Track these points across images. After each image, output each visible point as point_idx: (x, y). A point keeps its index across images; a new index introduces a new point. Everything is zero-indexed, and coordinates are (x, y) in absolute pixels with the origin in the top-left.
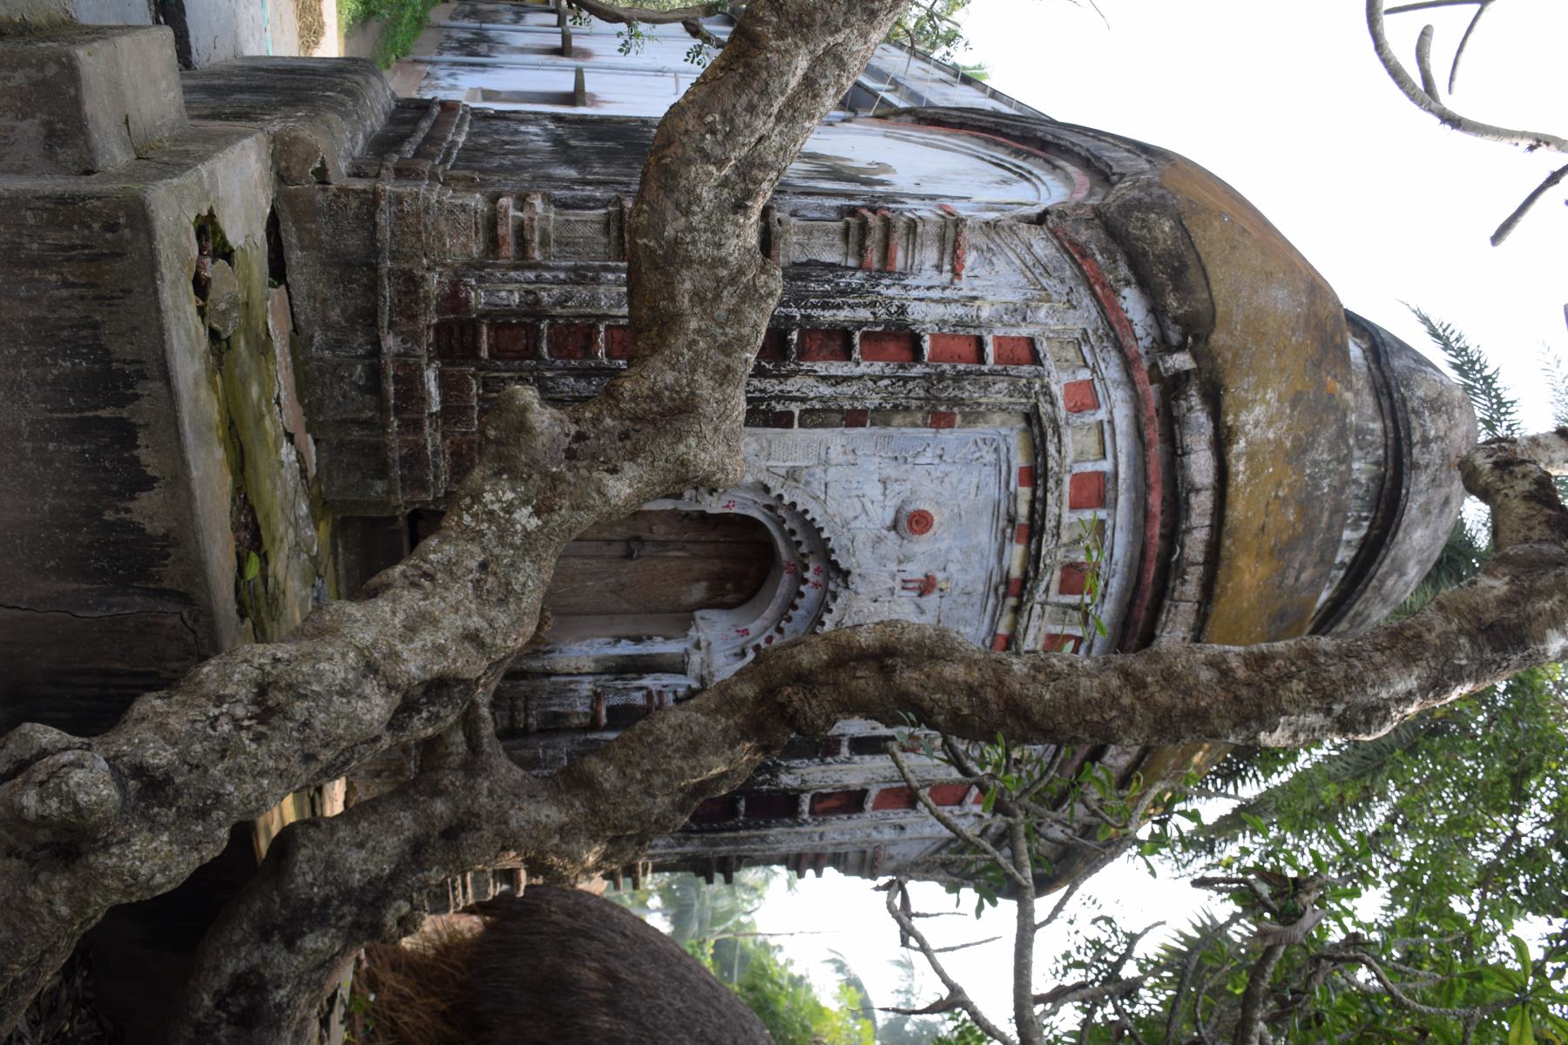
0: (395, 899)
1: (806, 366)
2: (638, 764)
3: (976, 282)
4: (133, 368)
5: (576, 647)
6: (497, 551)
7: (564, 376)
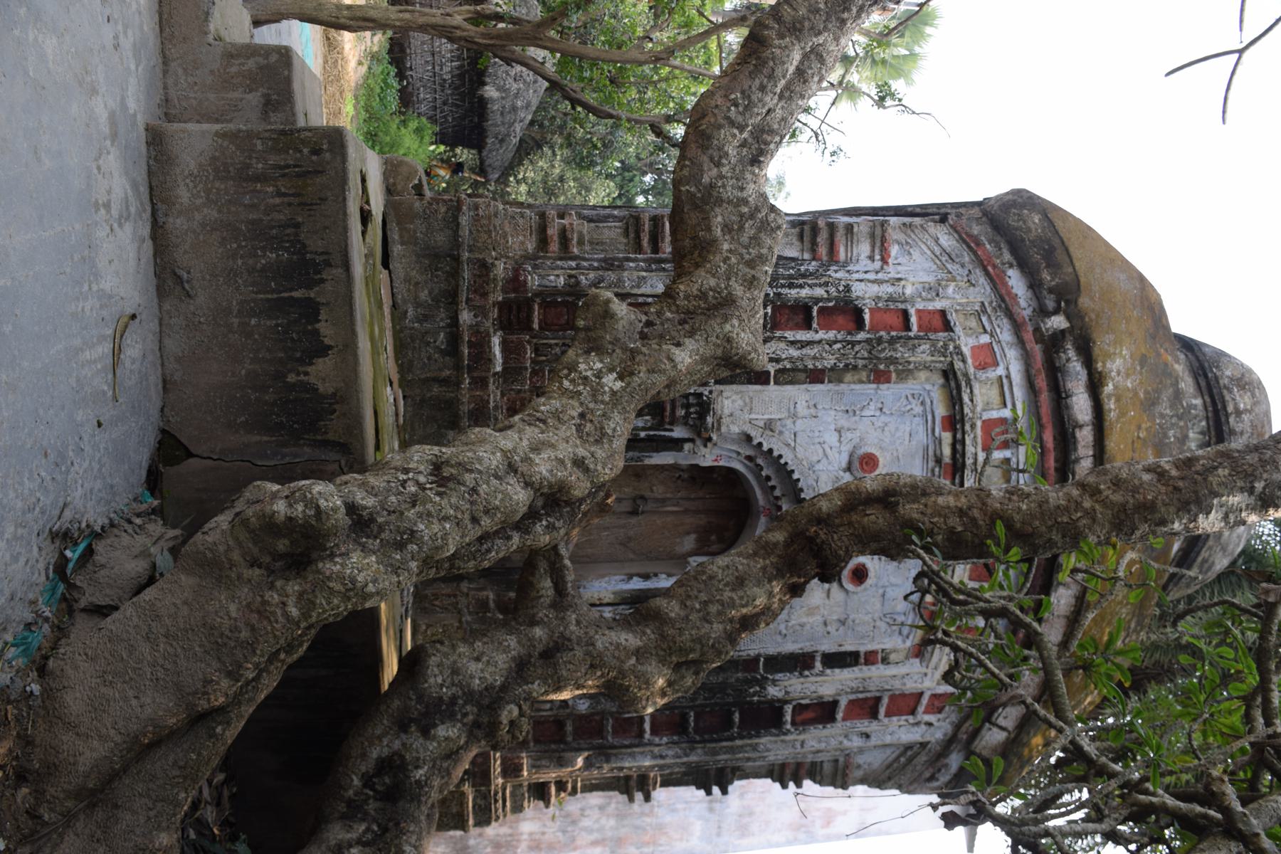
0: (508, 703)
1: (778, 334)
2: (697, 597)
3: (899, 268)
4: (322, 258)
5: (596, 584)
6: (592, 405)
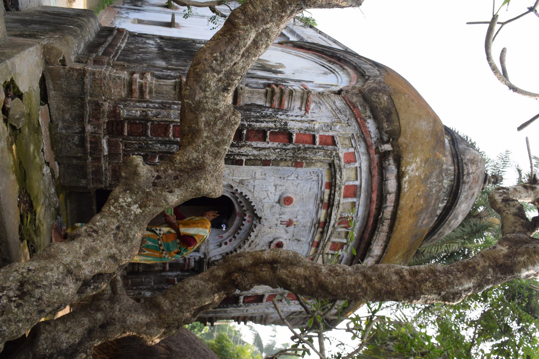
0: (80, 353)
1: (249, 143)
2: (178, 300)
3: (314, 115)
6: (124, 222)
7: (156, 143)
